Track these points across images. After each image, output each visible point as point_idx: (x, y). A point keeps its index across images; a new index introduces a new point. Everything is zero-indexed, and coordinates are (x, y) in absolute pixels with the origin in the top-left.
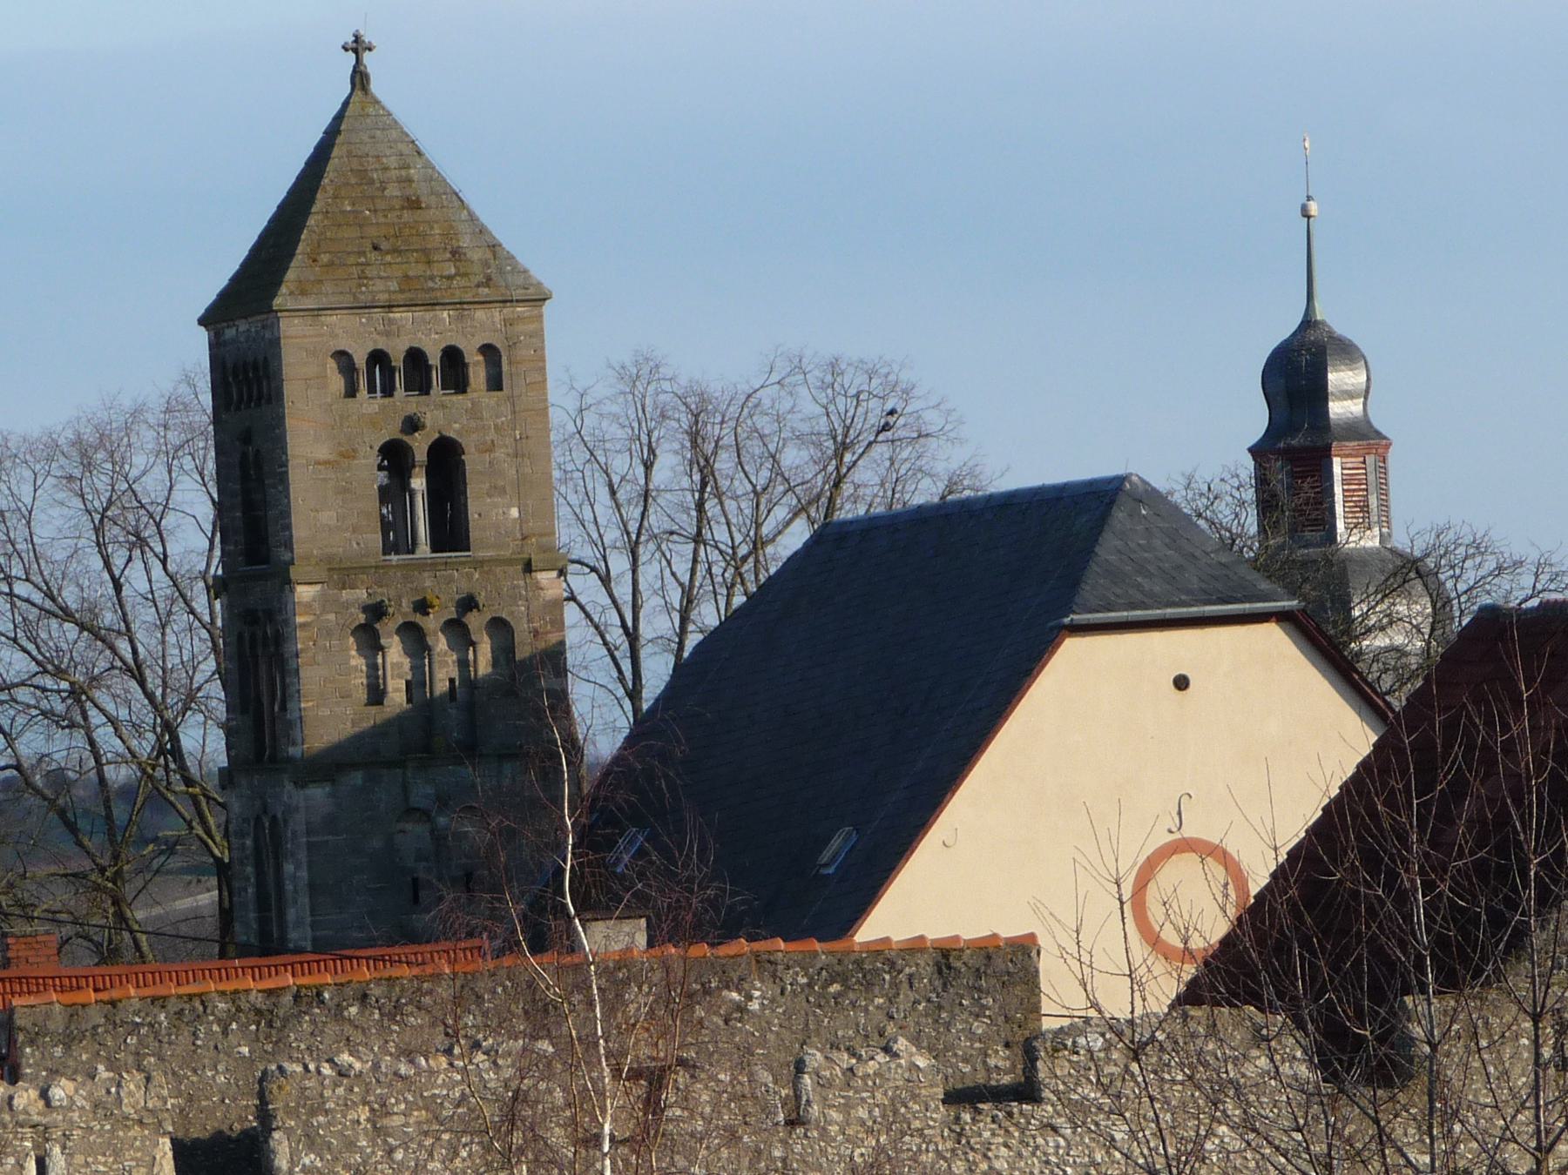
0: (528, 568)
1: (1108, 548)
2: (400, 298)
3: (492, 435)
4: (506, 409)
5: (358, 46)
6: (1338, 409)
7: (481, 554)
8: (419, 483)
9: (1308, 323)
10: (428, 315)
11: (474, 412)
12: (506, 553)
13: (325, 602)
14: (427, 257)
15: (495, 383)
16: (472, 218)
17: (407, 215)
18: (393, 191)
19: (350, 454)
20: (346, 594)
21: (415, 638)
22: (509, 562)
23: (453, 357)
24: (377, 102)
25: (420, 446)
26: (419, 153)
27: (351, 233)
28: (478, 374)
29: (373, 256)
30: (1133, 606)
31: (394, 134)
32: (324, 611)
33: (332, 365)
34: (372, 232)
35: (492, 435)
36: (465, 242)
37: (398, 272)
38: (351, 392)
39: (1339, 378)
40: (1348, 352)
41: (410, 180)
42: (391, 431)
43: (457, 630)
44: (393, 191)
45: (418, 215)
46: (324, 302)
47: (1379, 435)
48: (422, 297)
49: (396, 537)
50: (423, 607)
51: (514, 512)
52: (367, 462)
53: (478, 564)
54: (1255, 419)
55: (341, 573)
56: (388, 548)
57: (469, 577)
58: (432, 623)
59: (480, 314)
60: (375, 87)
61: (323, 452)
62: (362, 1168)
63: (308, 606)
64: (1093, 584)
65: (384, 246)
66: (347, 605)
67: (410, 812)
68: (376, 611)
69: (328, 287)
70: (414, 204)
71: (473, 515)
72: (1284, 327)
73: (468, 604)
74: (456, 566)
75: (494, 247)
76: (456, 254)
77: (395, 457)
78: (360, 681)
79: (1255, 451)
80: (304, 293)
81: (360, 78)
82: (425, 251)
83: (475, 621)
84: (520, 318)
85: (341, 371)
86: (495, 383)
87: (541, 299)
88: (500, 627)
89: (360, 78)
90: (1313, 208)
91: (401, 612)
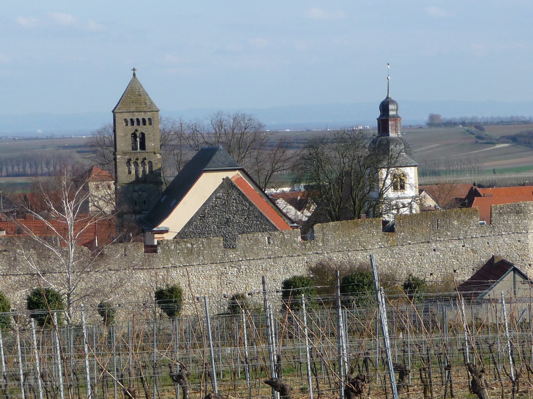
0: (155, 153)
1: (214, 158)
2: (135, 110)
3: (150, 132)
4: (152, 128)
5: (134, 70)
6: (391, 113)
7: (147, 151)
8: (138, 139)
9: (387, 98)
10: (140, 113)
11: (147, 128)
12: (152, 151)
13: (122, 158)
14: (141, 104)
15: (150, 124)
16: (149, 98)
17: (138, 97)
18: (137, 93)
19: (126, 135)
20: (125, 157)
21: (136, 164)
22: (152, 152)
23: (144, 120)
24: (136, 79)
25: (138, 134)
26: (142, 87)
27: (129, 100)
28: (147, 123)
29: (132, 104)
30: (215, 167)
31: (139, 84)
32: (122, 159)
33: (124, 122)
34: (132, 100)
35: (150, 132)
36: (147, 101)
37: (135, 106)
38: (127, 125)
39: (391, 107)
40: (393, 102)
41: (140, 91)
42: (133, 132)
43: (143, 162)
44: (137, 93)
45: (140, 97)
46: (122, 111)
47: (399, 117)
48: (138, 110)
49: (135, 148)
50: (137, 159)
51: (153, 144)
52: (129, 136)
53: (147, 152)
54: (378, 114)
55: (125, 153)
56: (133, 149)
57: (145, 154)
58: (139, 162)
59: (148, 113)
60: (136, 76)
61: (122, 135)
62: (327, 237)
63: (119, 159)
64: (211, 163)
65: (134, 102)
66: (125, 159)
67: (135, 191)
68: (130, 160)
69: (124, 108)
70: (140, 95)
71: (146, 145)
72: (383, 98)
73: (145, 159)
74: (143, 153)
75: (152, 102)
76: (145, 103)
77: (134, 136)
78: (127, 171)
79: (378, 119)
80: (119, 109)
81: (134, 75)
82: (141, 103)
83: (146, 162)
84: (155, 114)
85: (125, 122)
86: (150, 124)
87: (158, 111)
88: (150, 162)
89: (134, 75)
90: (389, 78)
91: (133, 160)
